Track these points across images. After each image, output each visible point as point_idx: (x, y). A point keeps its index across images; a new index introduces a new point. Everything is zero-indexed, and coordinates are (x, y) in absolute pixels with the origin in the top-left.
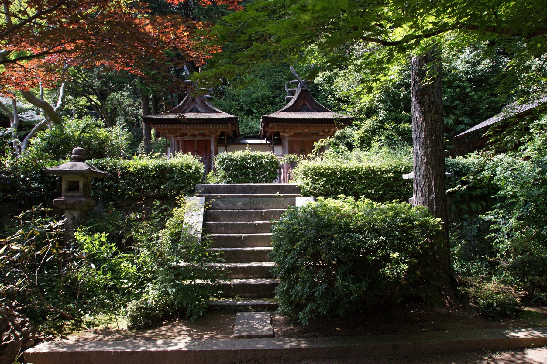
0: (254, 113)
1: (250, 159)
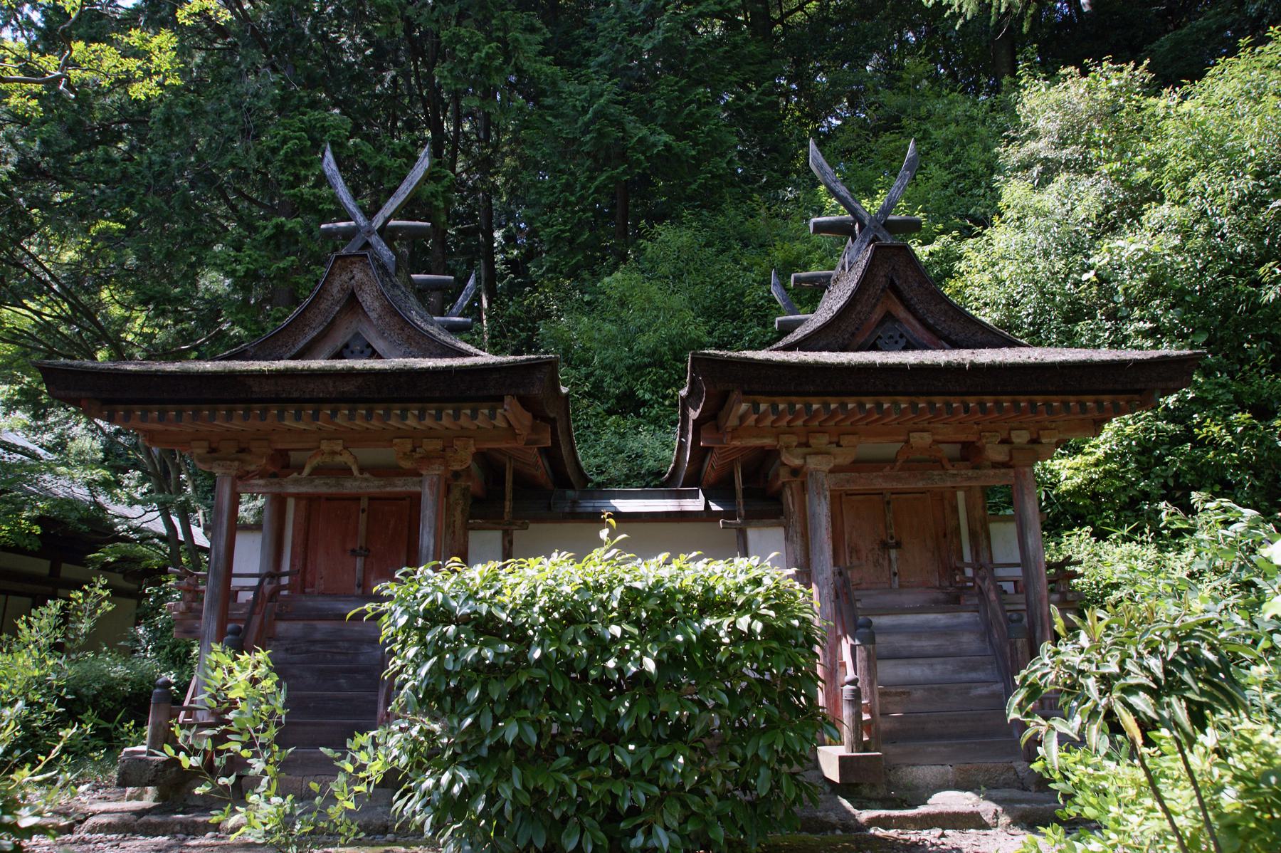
0: (644, 403)
1: (625, 616)
